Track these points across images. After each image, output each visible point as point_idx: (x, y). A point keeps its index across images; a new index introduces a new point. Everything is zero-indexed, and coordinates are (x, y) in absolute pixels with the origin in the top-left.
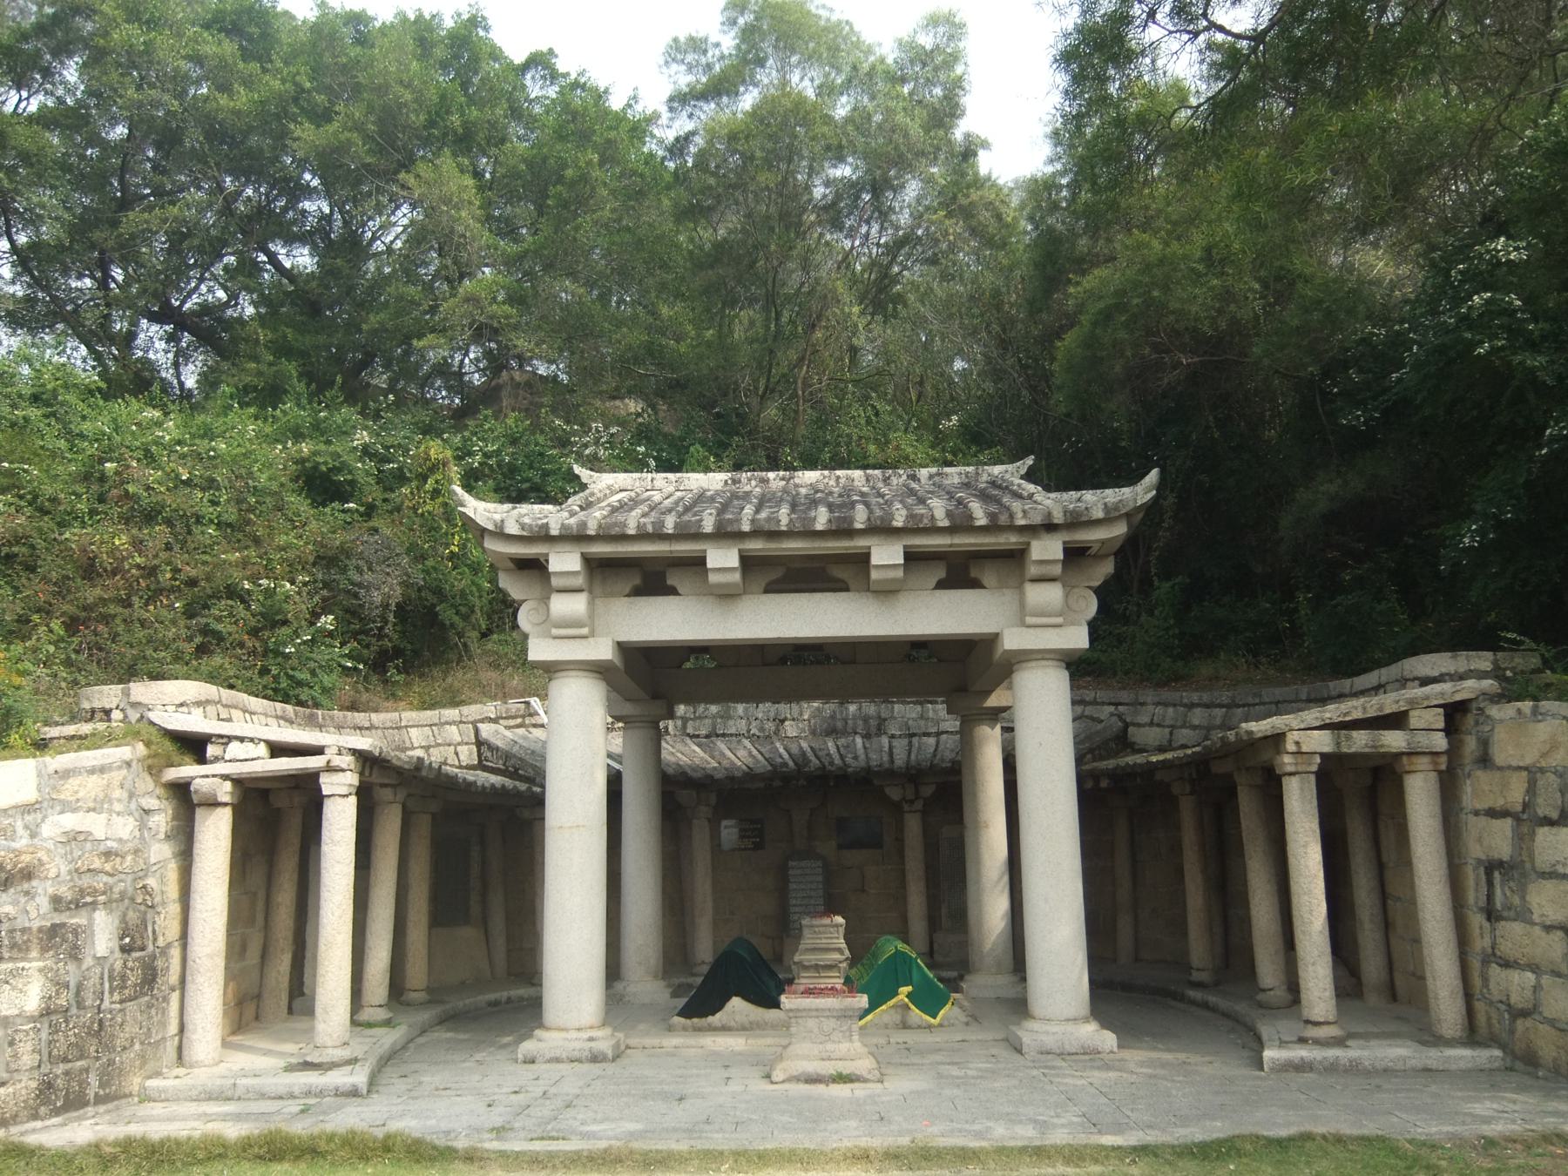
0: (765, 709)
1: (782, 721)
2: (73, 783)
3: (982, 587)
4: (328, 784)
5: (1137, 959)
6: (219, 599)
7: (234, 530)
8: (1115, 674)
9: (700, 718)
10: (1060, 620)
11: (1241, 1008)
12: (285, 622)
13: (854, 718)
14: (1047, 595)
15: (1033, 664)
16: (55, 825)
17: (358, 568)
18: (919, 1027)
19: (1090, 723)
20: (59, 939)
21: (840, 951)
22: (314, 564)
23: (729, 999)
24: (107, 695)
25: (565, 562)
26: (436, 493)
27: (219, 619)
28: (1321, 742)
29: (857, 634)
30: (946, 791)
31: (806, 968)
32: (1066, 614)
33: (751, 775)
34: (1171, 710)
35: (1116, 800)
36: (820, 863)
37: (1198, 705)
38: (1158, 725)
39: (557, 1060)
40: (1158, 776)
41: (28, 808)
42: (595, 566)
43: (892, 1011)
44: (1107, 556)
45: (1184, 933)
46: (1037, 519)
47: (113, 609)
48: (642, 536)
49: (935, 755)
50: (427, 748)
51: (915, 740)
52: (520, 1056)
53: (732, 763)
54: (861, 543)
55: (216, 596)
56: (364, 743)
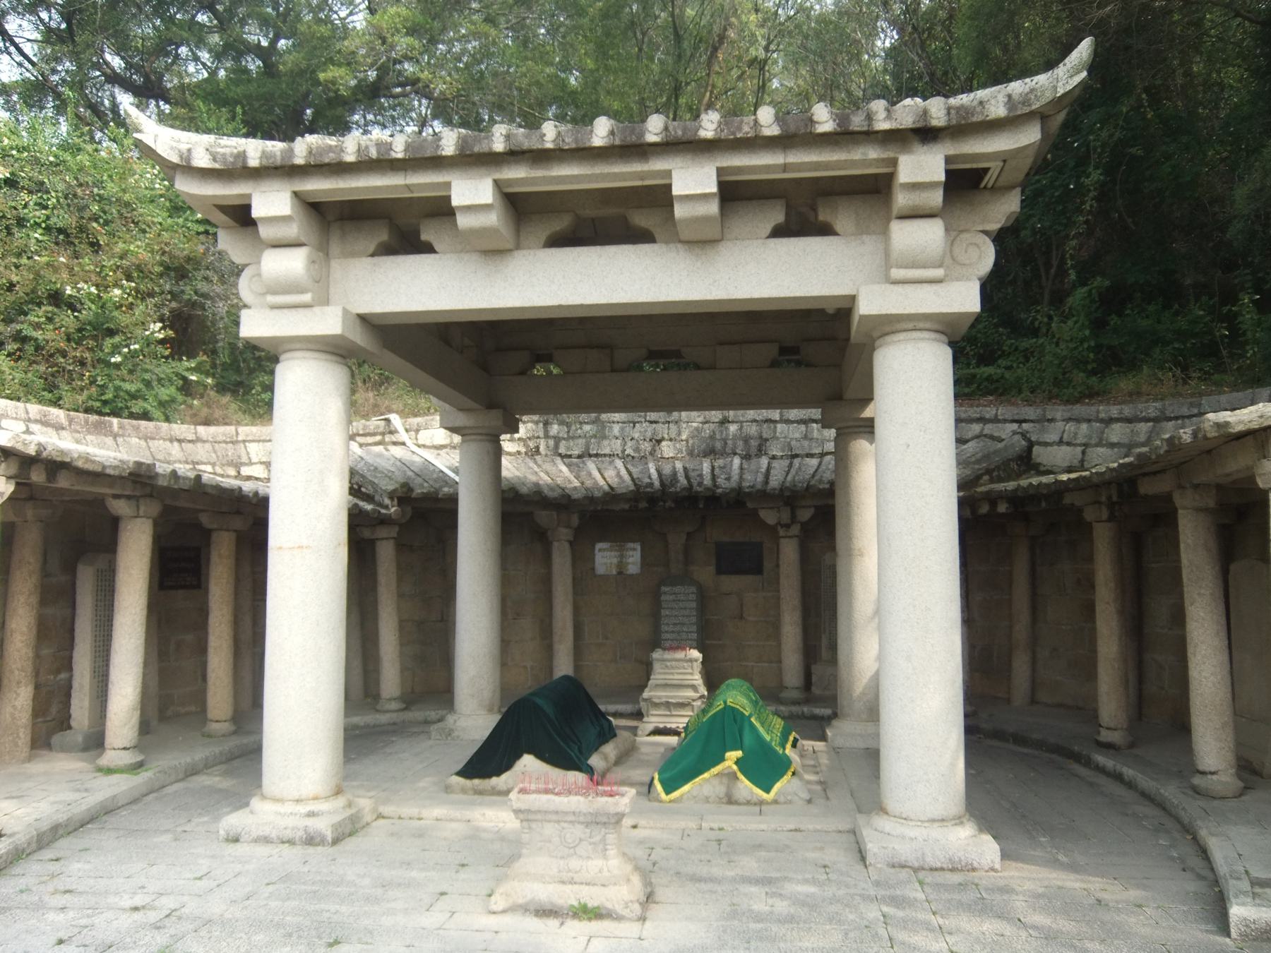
1: (659, 442)
3: (834, 233)
5: (1033, 701)
6: (39, 305)
8: (1020, 392)
9: (573, 438)
10: (939, 273)
11: (1170, 792)
13: (735, 438)
14: (924, 237)
15: (902, 336)
17: (206, 279)
18: (748, 803)
19: (989, 442)
21: (694, 688)
22: (161, 275)
23: (519, 756)
25: (272, 203)
27: (37, 326)
29: (662, 298)
30: (817, 516)
31: (656, 705)
32: (949, 263)
33: (611, 496)
34: (1084, 426)
35: (1003, 528)
36: (693, 589)
37: (1118, 420)
38: (1068, 444)
39: (266, 840)
40: (1068, 500)
43: (716, 782)
44: (1010, 188)
45: (1090, 674)
49: (813, 476)
51: (797, 462)
52: (222, 832)
53: (596, 483)
54: (658, 164)
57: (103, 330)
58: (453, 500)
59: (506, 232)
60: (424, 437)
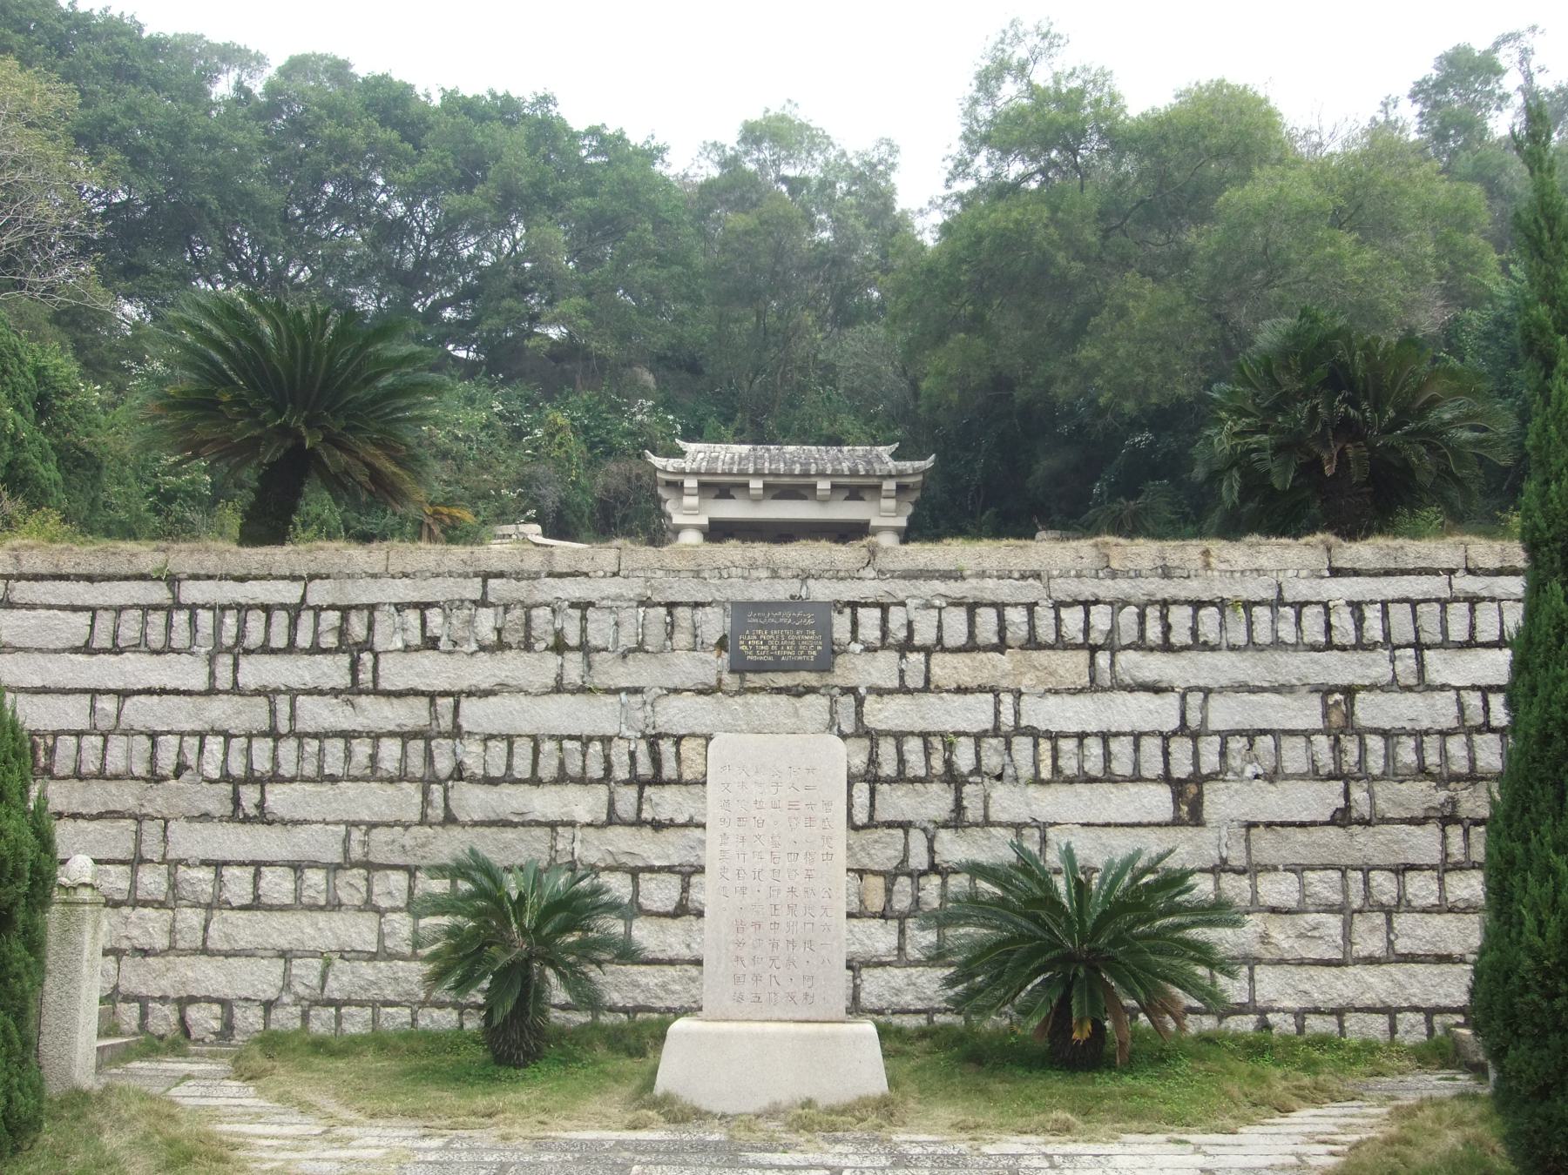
26: (560, 445)
32: (898, 512)
48: (724, 474)
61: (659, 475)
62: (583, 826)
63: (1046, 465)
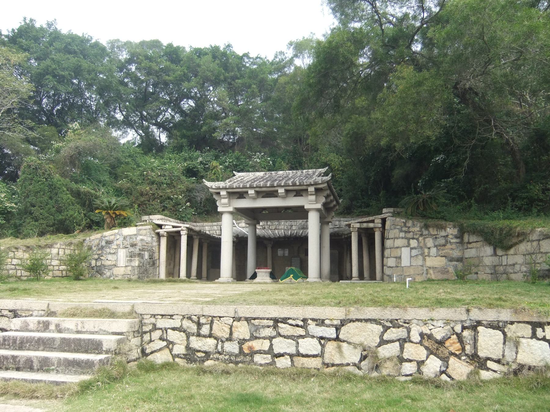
0: (288, 223)
2: (141, 231)
4: (182, 233)
7: (170, 185)
12: (180, 204)
16: (140, 237)
20: (140, 255)
24: (145, 218)
25: (223, 193)
26: (215, 174)
28: (358, 225)
32: (317, 202)
33: (280, 237)
41: (135, 235)
42: (229, 193)
46: (308, 183)
47: (146, 202)
48: (236, 188)
50: (209, 231)
54: (276, 188)
55: (166, 199)
56: (188, 226)
57: (177, 204)
58: (247, 238)
59: (256, 197)
60: (240, 225)
61: (210, 190)
62: (388, 267)
63: (398, 173)
